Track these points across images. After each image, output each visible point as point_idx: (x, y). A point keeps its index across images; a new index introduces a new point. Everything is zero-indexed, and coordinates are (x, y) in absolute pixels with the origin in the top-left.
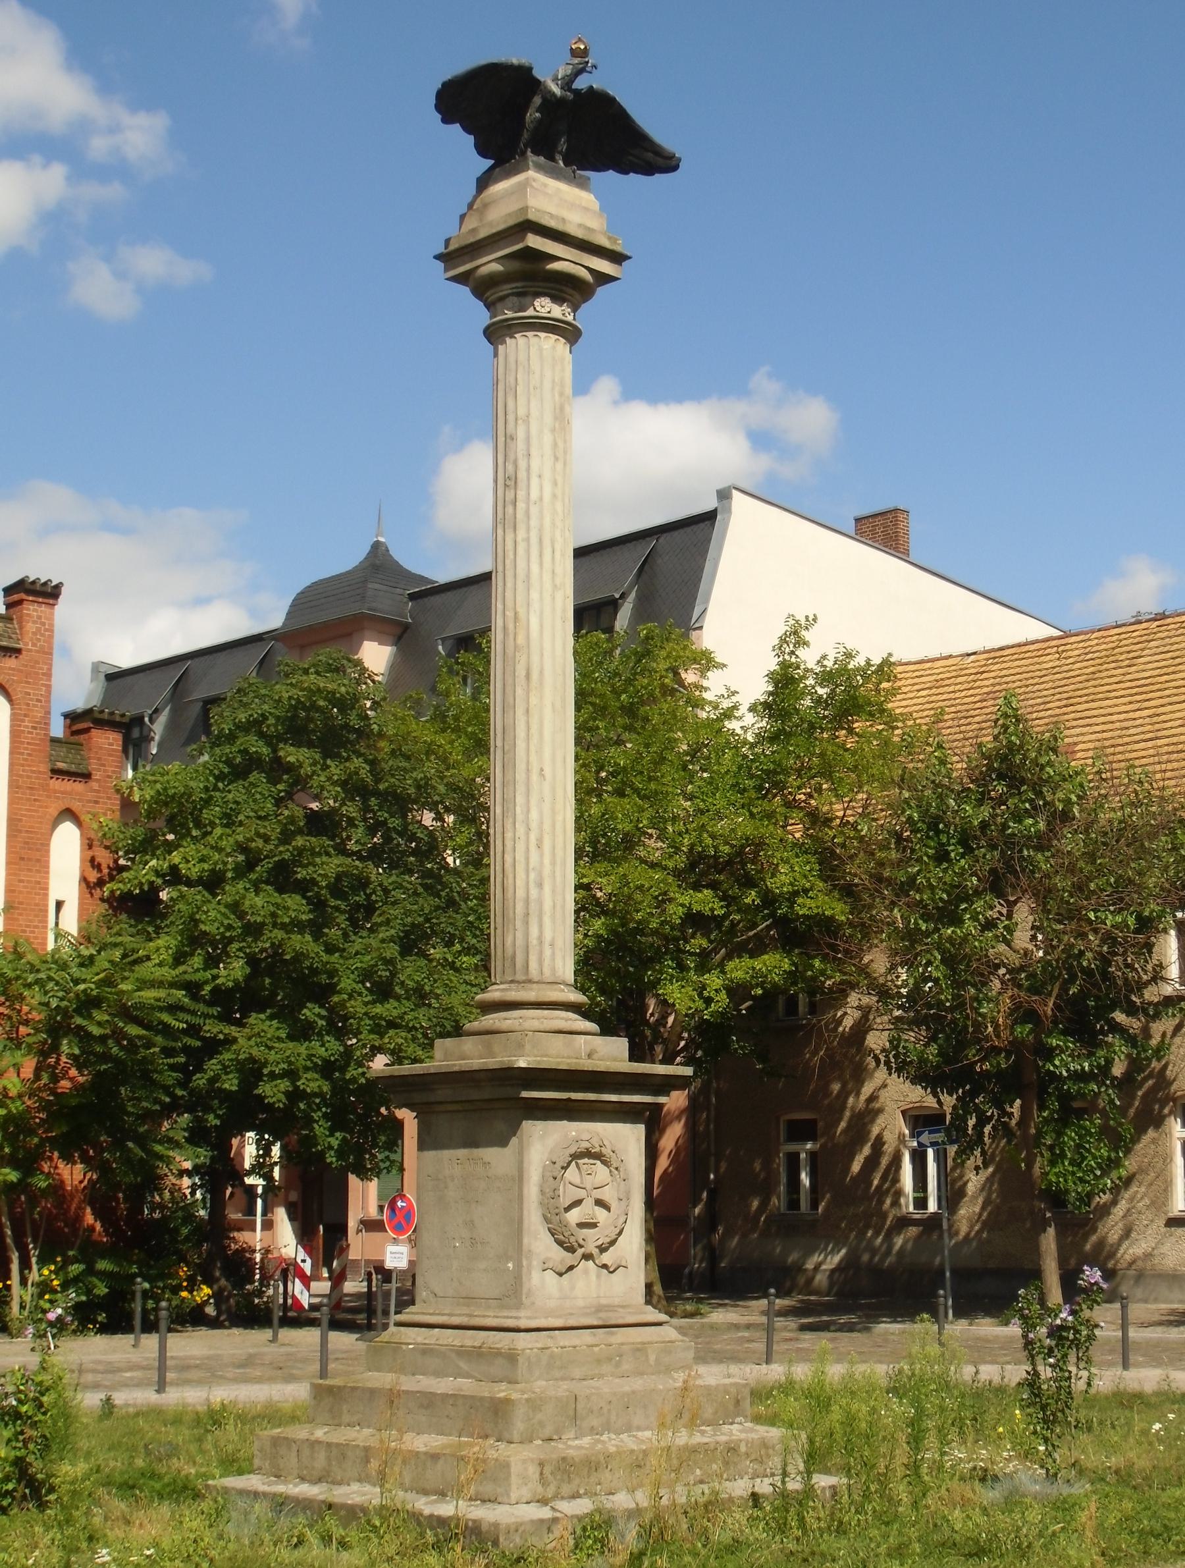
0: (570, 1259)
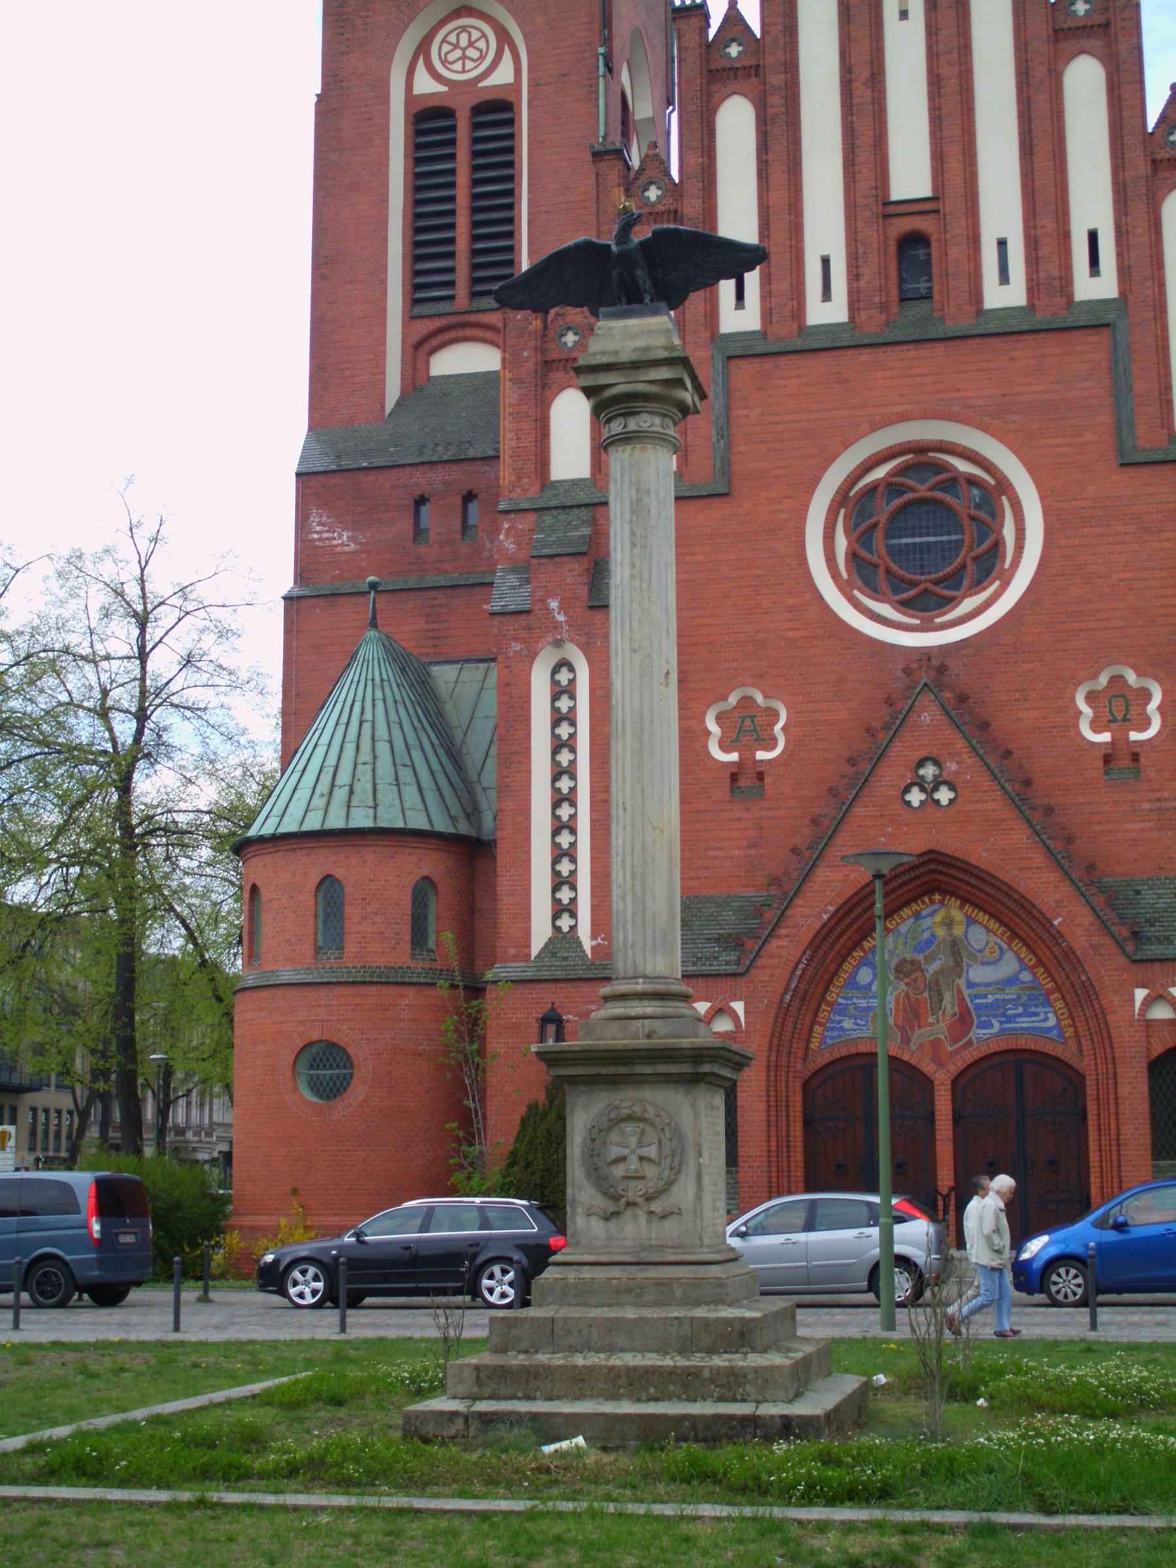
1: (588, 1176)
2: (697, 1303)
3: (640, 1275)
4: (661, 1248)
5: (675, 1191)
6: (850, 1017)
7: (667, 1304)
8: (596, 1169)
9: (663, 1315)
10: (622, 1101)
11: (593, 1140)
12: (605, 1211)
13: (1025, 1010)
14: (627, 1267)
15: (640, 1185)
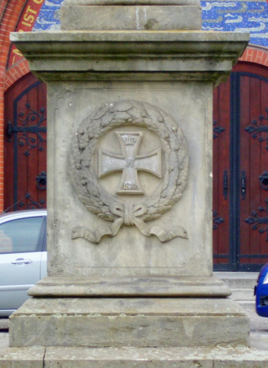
0: (103, 229)
1: (74, 190)
2: (212, 343)
3: (141, 310)
4: (162, 278)
5: (180, 210)
6: (58, 22)
7: (175, 345)
8: (85, 184)
9: (178, 358)
10: (116, 104)
11: (82, 149)
12: (94, 234)
13: (245, 20)
14: (123, 300)
15: (139, 202)
